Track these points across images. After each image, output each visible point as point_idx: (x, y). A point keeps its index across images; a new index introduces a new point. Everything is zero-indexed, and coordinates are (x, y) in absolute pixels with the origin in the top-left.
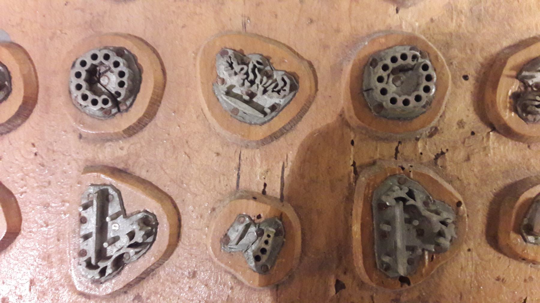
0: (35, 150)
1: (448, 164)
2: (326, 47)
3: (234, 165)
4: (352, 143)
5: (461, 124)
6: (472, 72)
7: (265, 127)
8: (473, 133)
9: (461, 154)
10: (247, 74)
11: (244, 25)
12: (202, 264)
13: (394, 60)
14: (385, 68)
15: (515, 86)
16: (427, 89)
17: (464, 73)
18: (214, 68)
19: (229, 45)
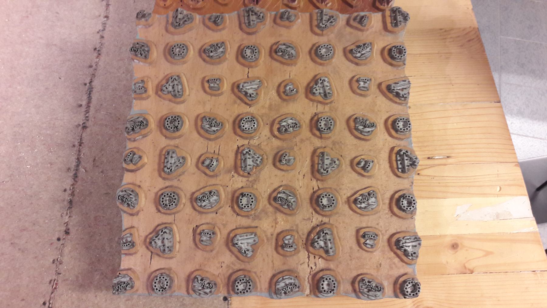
0: (153, 141)
1: (262, 146)
2: (231, 116)
3: (207, 145)
4: (238, 140)
5: (266, 136)
6: (268, 123)
7: (215, 135)
8: (269, 138)
9: (265, 143)
10: (210, 121)
11: (210, 111)
12: (164, 286)
13: (246, 119)
14: (244, 121)
15: (278, 126)
16: (254, 126)
17: (266, 123)
18: (296, 53)
19: (410, 20)
